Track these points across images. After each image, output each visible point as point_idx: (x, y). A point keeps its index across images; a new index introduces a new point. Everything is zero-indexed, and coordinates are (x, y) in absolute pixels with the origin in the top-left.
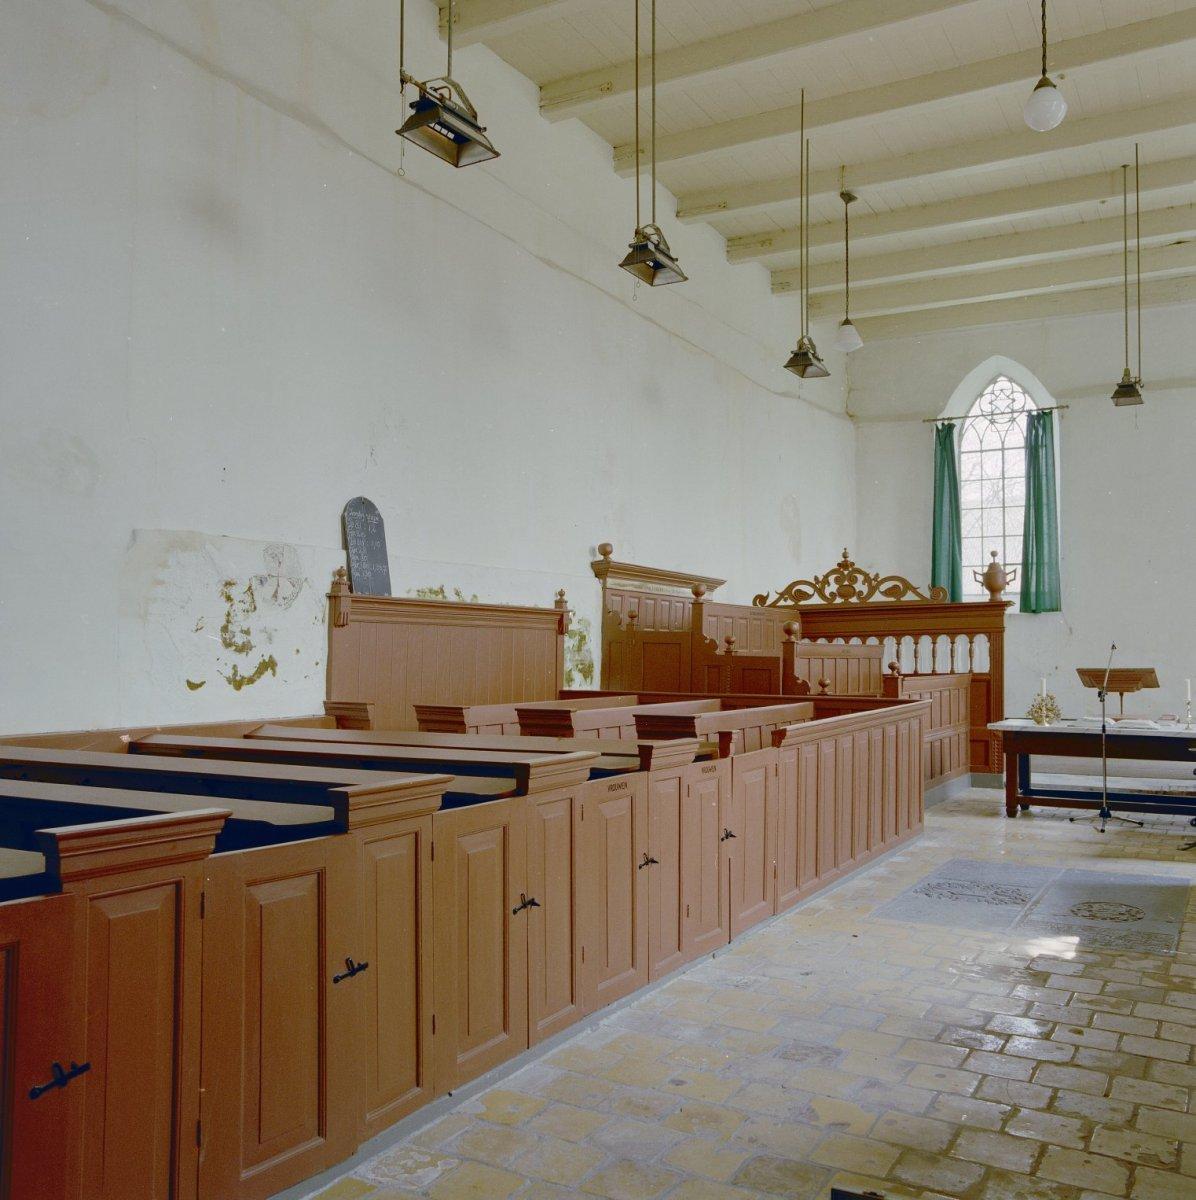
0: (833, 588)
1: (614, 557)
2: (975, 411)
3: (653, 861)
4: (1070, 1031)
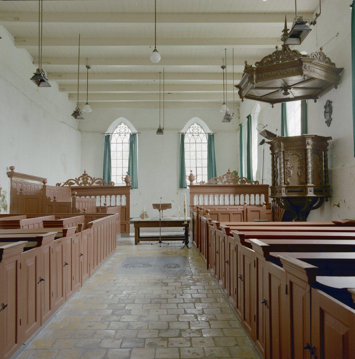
1: (15, 171)
2: (115, 132)
3: (67, 264)
4: (180, 295)
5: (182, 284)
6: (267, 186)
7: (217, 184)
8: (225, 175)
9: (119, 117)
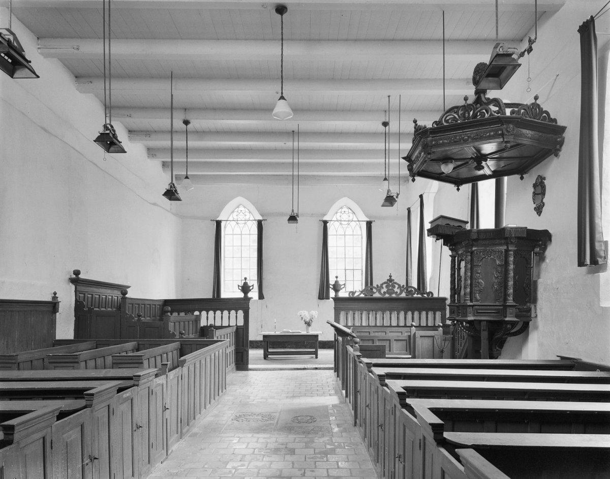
0: (385, 290)
1: (81, 276)
4: (311, 471)
5: (316, 451)
6: (444, 299)
7: (372, 295)
9: (232, 198)
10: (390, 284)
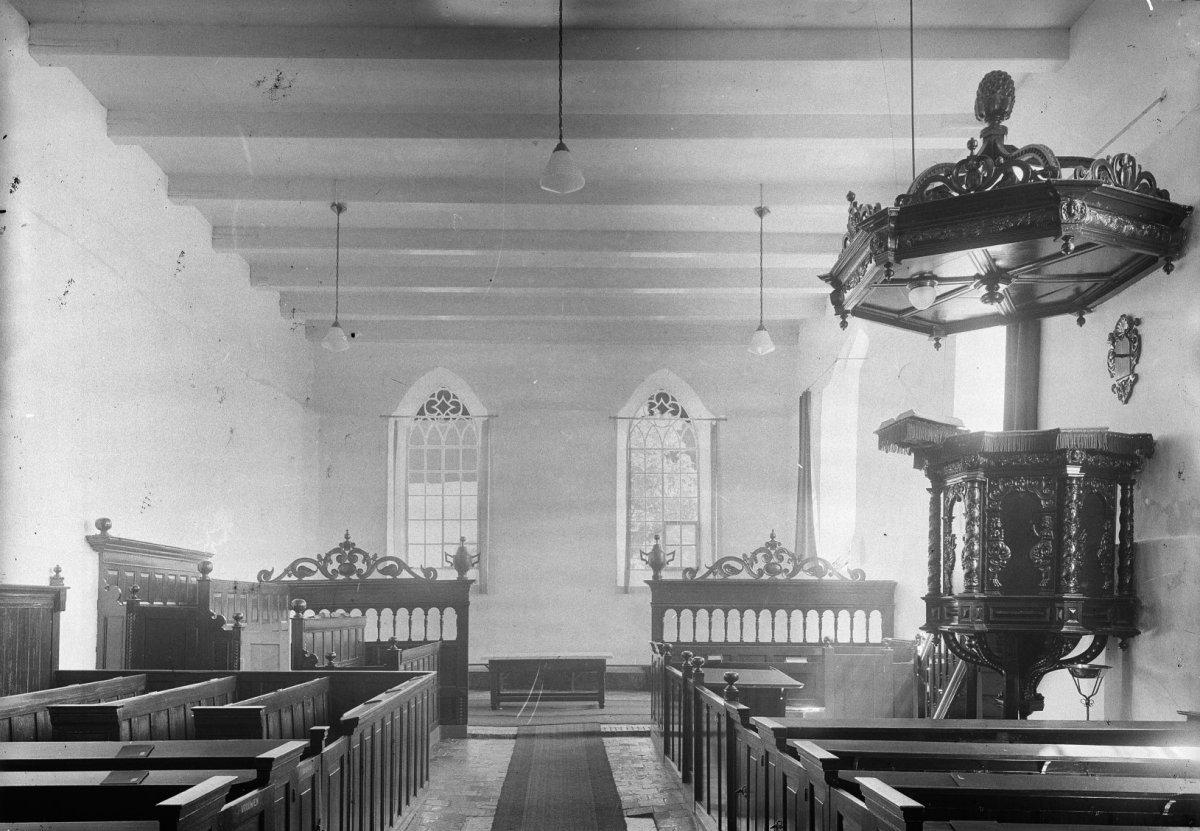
0: (335, 565)
8: (760, 550)
10: (347, 552)
